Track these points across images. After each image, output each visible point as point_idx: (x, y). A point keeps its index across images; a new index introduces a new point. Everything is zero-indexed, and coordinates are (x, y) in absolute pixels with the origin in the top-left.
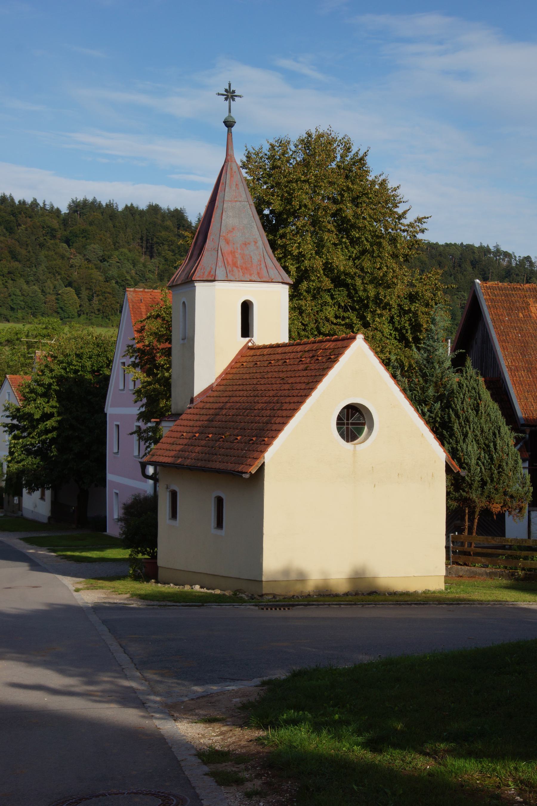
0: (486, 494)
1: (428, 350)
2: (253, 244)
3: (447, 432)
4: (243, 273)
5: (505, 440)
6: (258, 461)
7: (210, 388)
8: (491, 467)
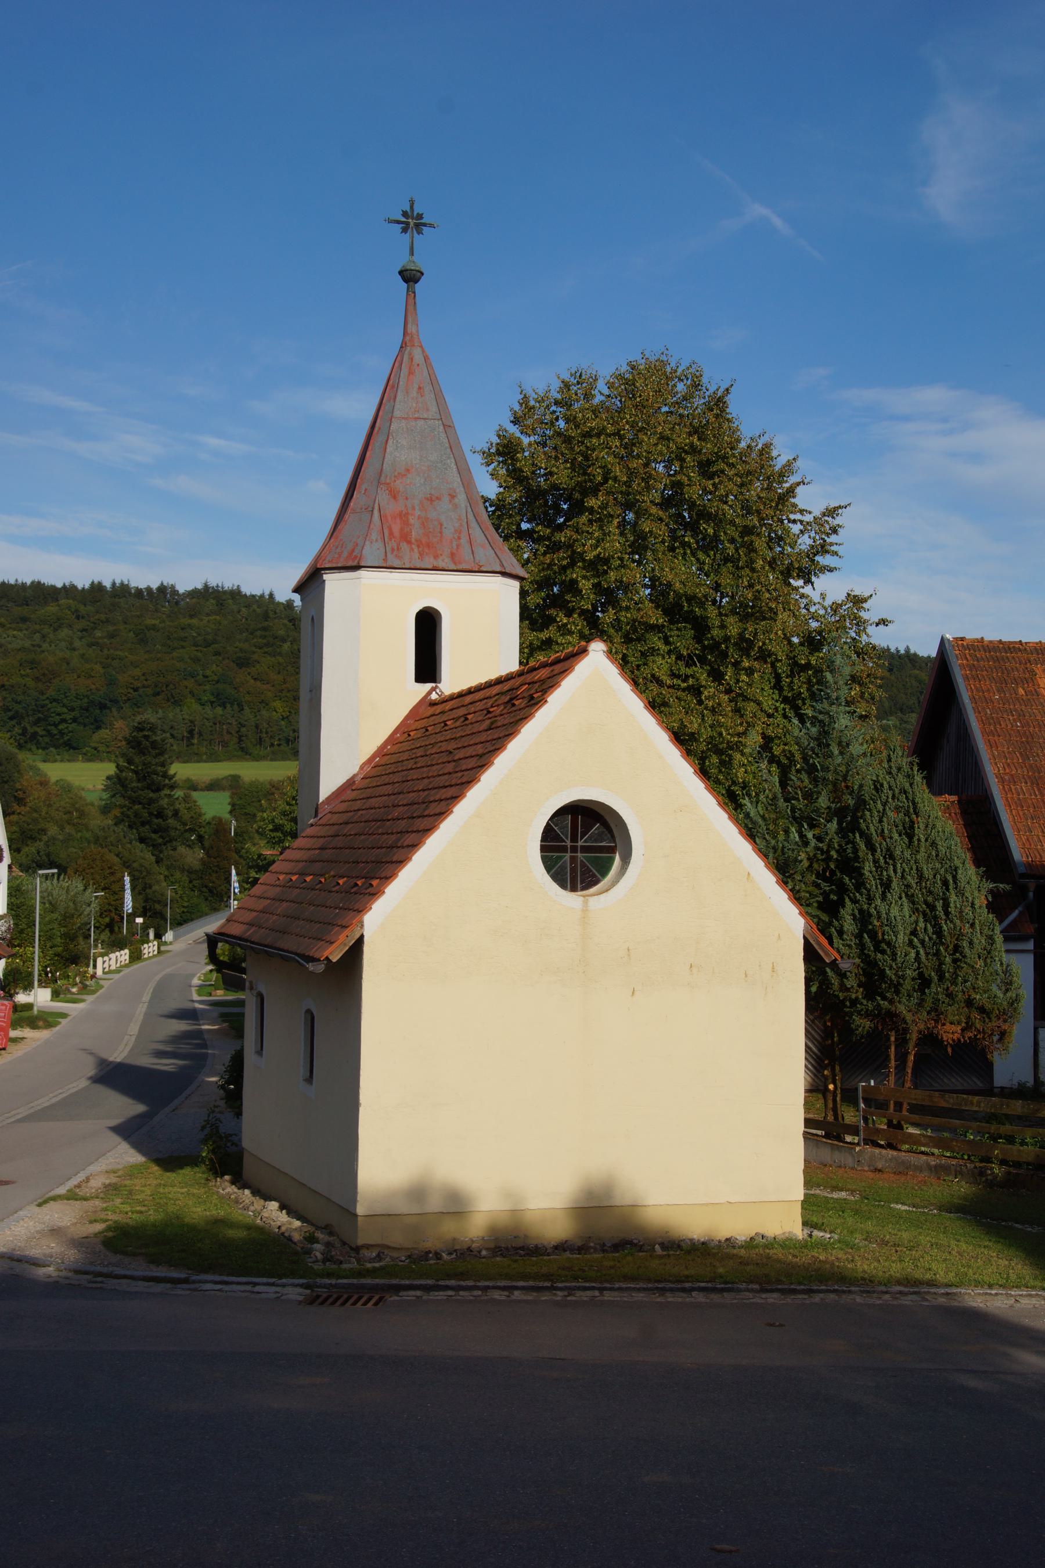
0: (928, 1005)
1: (820, 721)
2: (446, 499)
3: (850, 880)
4: (421, 555)
5: (968, 894)
6: (347, 932)
7: (350, 784)
8: (938, 950)
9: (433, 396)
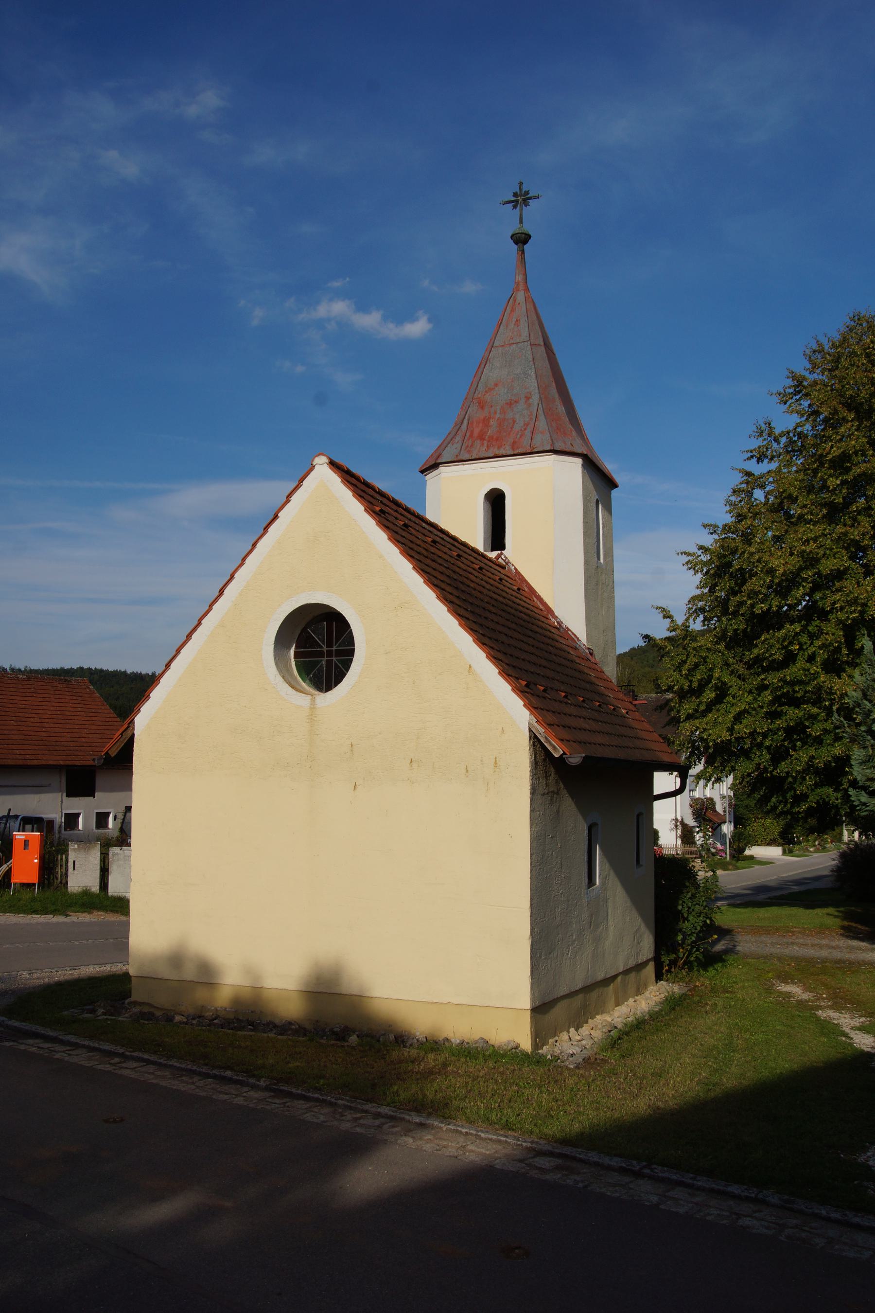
9: (526, 325)
